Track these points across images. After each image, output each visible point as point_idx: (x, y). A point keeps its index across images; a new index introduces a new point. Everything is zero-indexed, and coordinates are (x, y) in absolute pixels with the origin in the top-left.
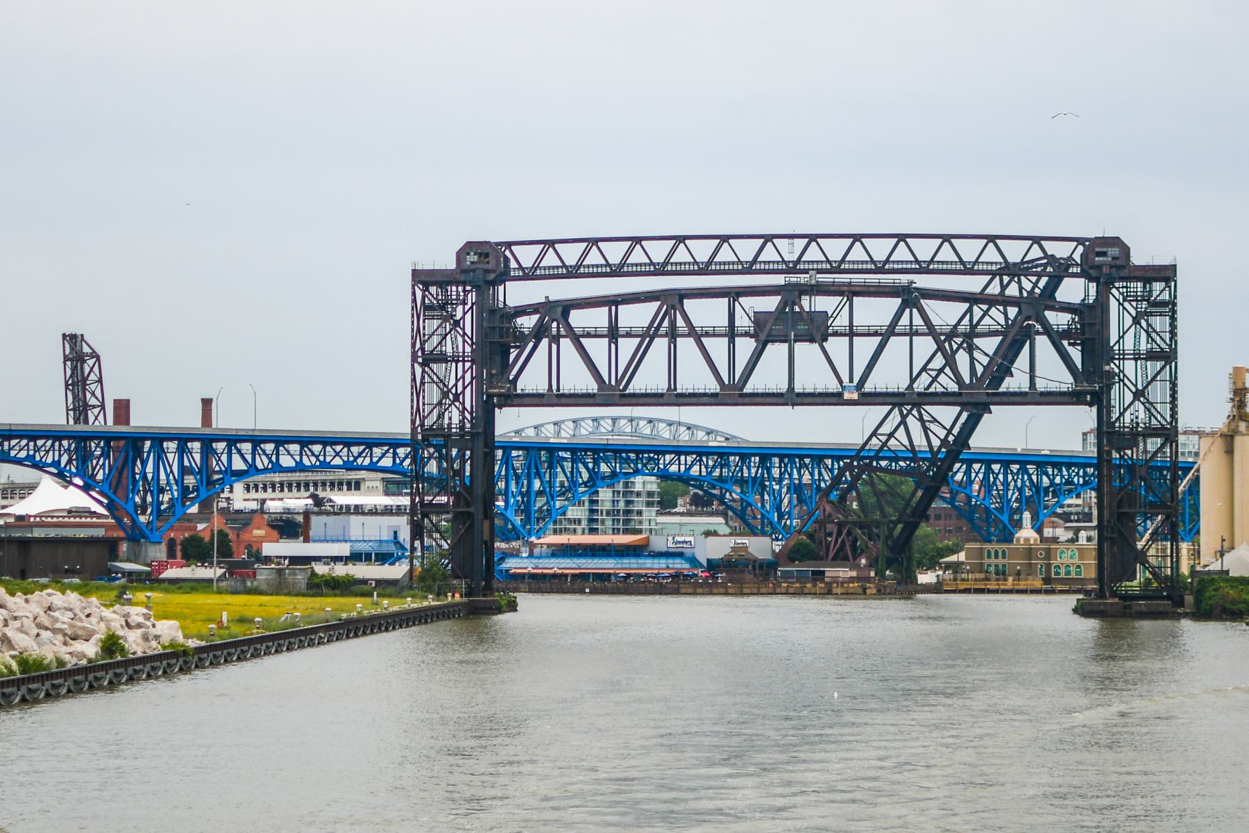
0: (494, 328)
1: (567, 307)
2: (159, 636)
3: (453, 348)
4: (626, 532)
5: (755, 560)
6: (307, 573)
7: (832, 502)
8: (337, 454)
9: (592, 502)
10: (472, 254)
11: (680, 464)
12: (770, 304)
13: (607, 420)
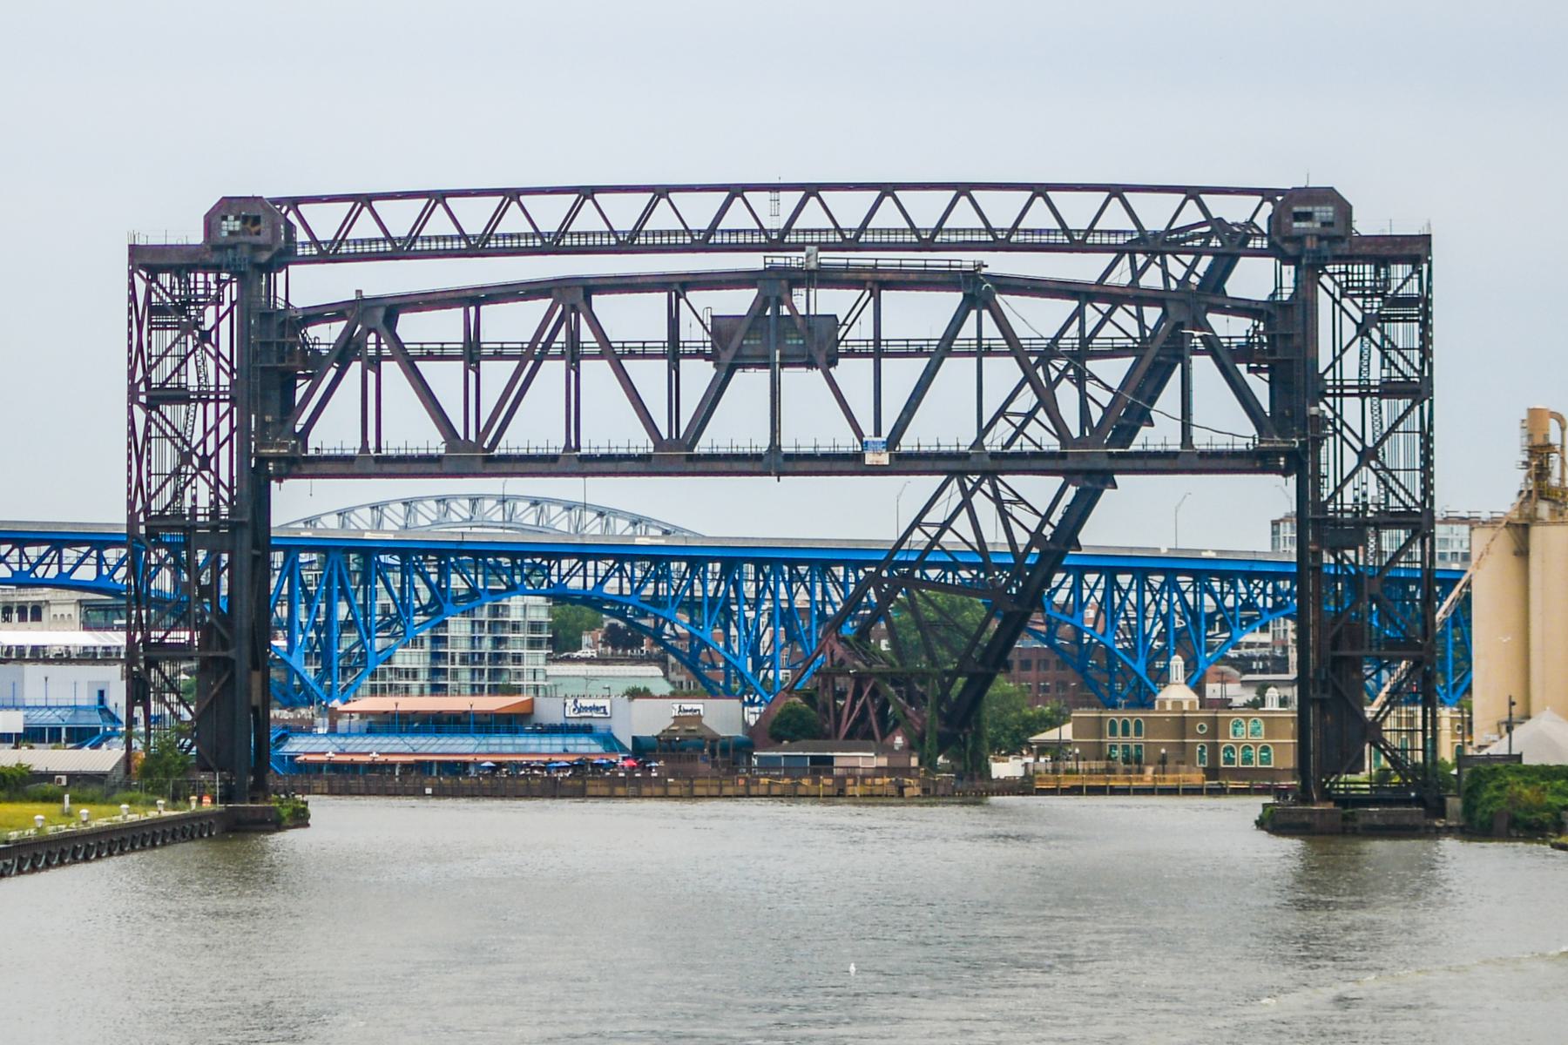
1: (393, 308)
3: (199, 379)
4: (495, 690)
5: (715, 739)
7: (845, 640)
9: (436, 640)
10: (231, 218)
11: (585, 576)
12: (739, 302)
13: (460, 501)
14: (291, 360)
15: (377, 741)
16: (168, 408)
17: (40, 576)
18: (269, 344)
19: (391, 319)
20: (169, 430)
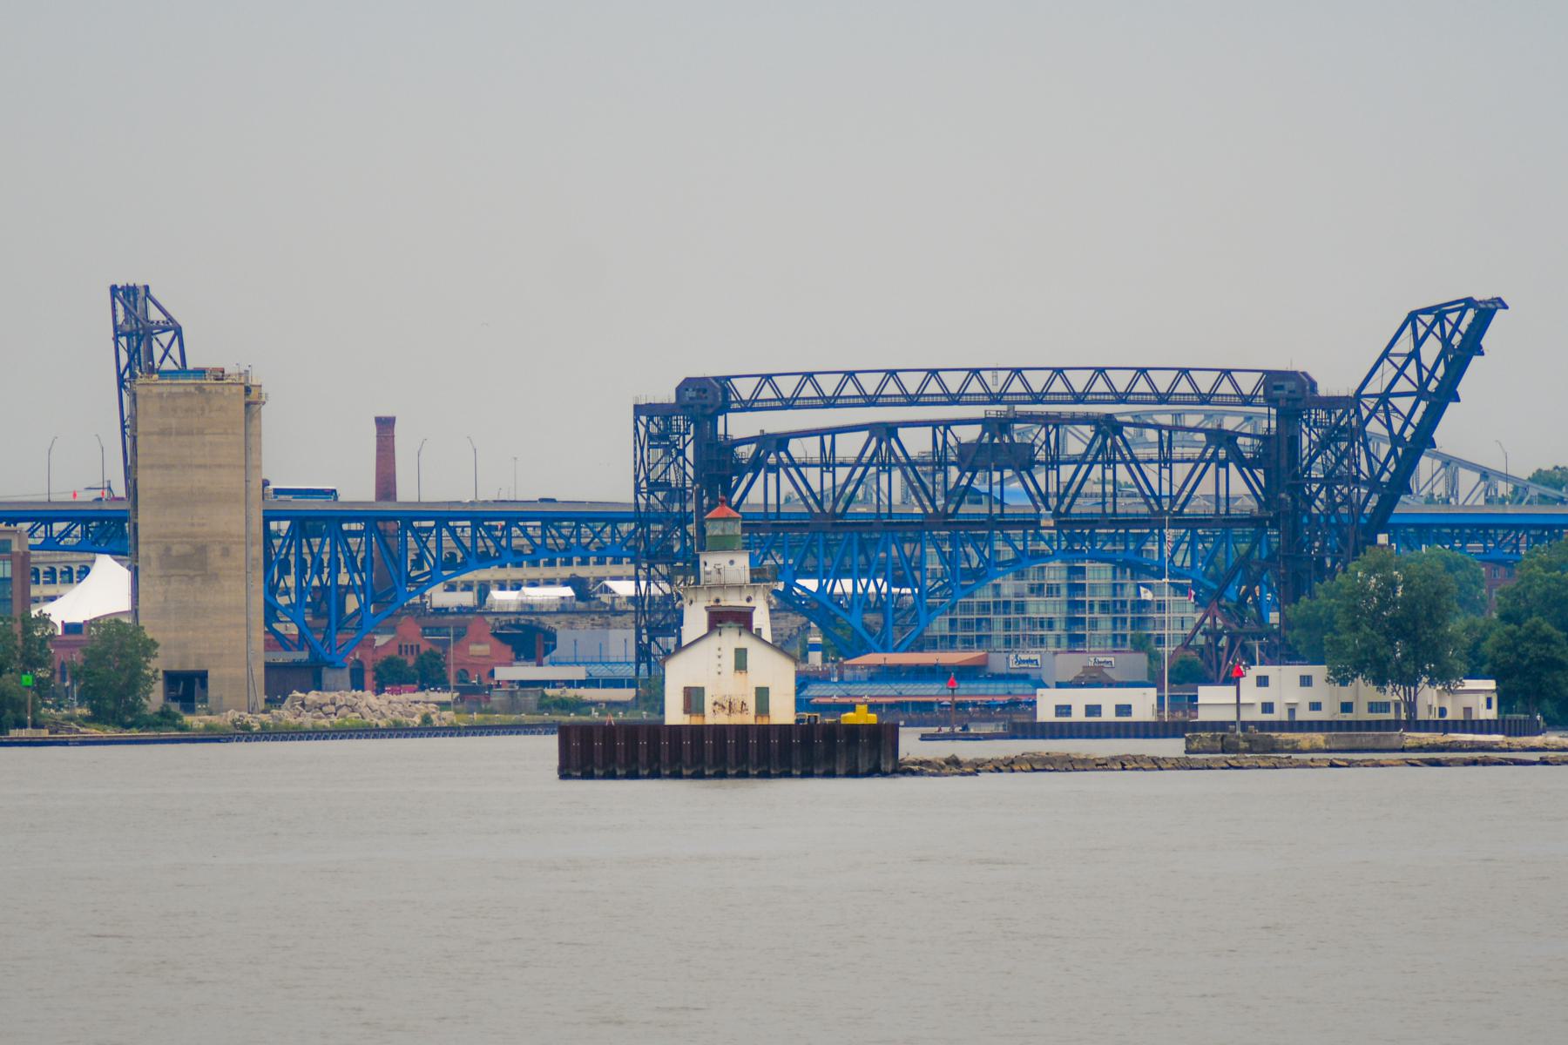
8: (597, 535)
9: (1075, 588)
10: (690, 390)
12: (970, 434)
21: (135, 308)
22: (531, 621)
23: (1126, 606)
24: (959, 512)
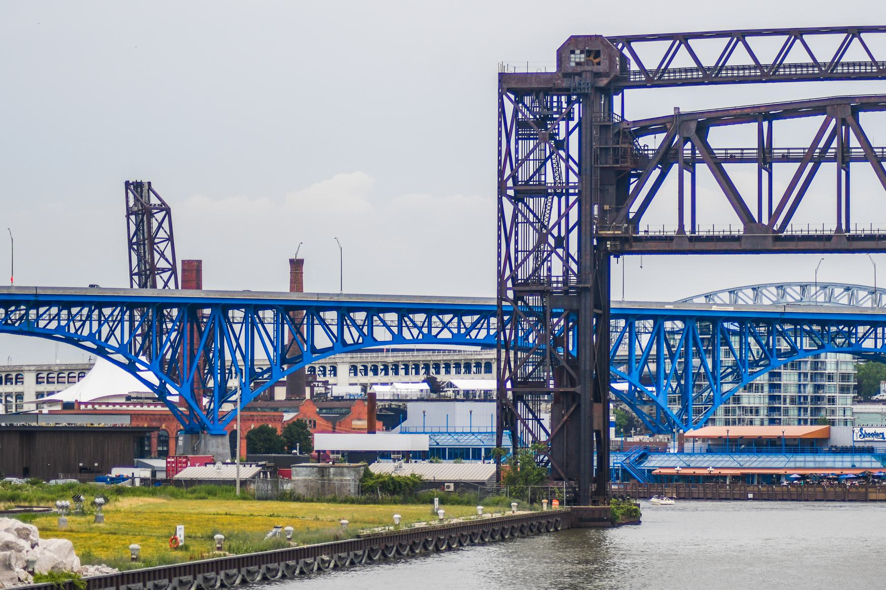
0: (607, 150)
2: (33, 562)
3: (554, 179)
4: (814, 422)
6: (358, 472)
9: (772, 386)
10: (578, 52)
11: (876, 338)
13: (794, 288)
14: (623, 162)
15: (713, 459)
16: (531, 200)
17: (473, 337)
18: (607, 149)
19: (702, 130)
20: (531, 218)
21: (142, 197)
22: (400, 406)
23: (807, 400)
24: (650, 353)
